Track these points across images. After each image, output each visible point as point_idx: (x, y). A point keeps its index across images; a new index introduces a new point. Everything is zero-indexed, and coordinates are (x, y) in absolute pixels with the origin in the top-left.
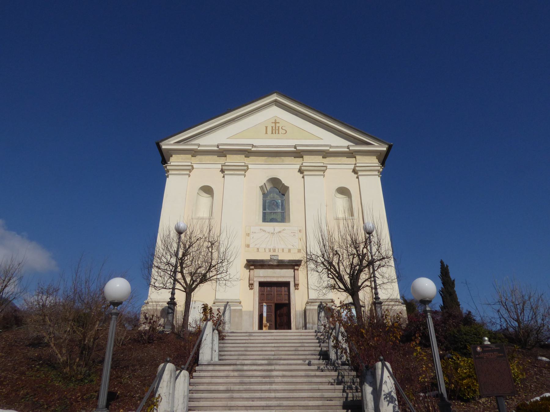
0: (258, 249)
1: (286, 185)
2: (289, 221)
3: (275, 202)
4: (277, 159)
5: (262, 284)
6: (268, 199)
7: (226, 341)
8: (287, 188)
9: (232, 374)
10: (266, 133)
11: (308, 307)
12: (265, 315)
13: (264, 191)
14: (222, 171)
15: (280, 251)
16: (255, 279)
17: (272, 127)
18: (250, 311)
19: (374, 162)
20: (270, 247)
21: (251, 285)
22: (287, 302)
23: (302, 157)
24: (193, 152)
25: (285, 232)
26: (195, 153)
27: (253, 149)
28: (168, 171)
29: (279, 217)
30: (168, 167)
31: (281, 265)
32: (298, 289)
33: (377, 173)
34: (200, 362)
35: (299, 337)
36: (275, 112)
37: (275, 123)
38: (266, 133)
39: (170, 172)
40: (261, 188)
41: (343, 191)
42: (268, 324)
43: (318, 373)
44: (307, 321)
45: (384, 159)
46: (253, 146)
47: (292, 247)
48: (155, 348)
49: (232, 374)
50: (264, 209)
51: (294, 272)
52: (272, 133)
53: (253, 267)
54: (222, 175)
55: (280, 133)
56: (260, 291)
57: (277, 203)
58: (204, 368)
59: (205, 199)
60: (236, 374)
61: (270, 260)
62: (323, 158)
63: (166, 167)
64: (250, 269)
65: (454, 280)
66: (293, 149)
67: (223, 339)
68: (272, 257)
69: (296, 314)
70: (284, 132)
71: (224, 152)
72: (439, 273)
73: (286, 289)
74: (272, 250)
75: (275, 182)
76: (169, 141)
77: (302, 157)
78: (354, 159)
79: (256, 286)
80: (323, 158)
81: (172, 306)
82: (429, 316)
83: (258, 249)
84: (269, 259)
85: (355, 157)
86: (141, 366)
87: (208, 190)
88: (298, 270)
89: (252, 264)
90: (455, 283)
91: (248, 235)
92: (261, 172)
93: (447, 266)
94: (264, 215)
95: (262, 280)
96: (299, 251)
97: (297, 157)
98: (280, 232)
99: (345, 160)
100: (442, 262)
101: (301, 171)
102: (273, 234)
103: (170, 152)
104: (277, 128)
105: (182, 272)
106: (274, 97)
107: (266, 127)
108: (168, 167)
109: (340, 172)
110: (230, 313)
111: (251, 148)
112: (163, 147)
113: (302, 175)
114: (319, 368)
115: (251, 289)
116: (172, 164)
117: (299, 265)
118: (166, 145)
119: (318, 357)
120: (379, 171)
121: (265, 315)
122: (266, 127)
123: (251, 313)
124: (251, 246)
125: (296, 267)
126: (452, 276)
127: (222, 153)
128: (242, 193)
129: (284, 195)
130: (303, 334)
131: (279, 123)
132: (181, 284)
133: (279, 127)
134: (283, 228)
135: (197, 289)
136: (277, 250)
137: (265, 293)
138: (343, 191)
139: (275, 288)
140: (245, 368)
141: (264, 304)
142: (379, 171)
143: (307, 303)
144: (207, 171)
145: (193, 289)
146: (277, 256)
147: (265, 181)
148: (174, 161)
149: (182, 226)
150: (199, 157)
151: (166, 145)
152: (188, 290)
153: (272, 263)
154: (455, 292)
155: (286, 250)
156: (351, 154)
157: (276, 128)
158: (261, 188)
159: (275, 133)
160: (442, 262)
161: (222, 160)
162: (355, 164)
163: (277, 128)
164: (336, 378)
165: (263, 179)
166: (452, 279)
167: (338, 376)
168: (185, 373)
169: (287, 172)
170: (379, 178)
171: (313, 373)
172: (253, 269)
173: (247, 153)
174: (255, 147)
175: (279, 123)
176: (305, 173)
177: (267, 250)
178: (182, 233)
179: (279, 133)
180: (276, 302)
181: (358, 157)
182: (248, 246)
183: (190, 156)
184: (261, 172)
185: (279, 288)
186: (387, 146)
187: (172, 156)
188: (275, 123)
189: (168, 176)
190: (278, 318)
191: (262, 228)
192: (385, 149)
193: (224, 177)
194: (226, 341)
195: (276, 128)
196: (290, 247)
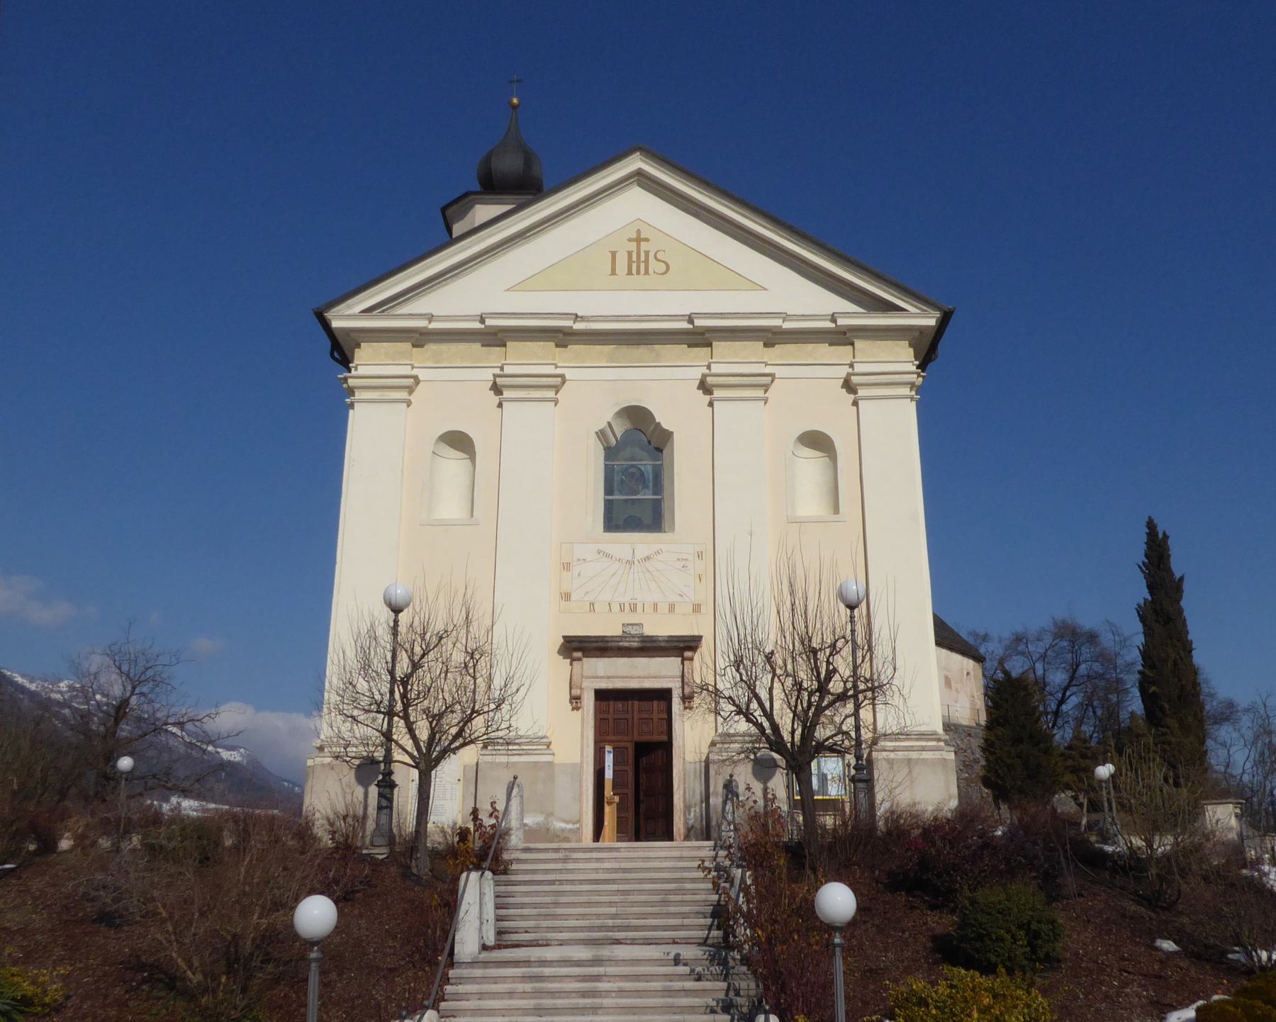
0: (592, 604)
1: (665, 426)
2: (672, 529)
3: (636, 478)
4: (641, 351)
5: (601, 695)
6: (618, 464)
7: (513, 878)
8: (668, 436)
9: (520, 987)
10: (613, 272)
11: (713, 757)
12: (609, 774)
14: (496, 389)
15: (649, 609)
16: (585, 684)
17: (630, 254)
18: (574, 765)
19: (902, 359)
20: (622, 600)
21: (575, 700)
22: (665, 738)
23: (710, 345)
24: (417, 336)
25: (659, 557)
26: (419, 338)
27: (579, 326)
28: (351, 392)
29: (647, 518)
30: (351, 382)
31: (650, 647)
32: (691, 708)
33: (906, 391)
34: (456, 958)
35: (677, 862)
36: (637, 207)
37: (639, 240)
38: (613, 272)
39: (359, 395)
40: (601, 435)
41: (817, 441)
42: (617, 799)
43: (690, 985)
44: (711, 790)
45: (928, 350)
47: (679, 599)
48: (361, 916)
49: (520, 987)
50: (609, 490)
51: (683, 663)
52: (630, 273)
53: (579, 654)
54: (496, 399)
55: (651, 271)
56: (598, 711)
57: (642, 474)
58: (465, 972)
59: (453, 463)
60: (528, 987)
61: (621, 638)
62: (766, 345)
63: (345, 379)
64: (573, 660)
65: (1181, 579)
66: (685, 325)
67: (505, 872)
68: (628, 629)
69: (684, 769)
70: (663, 267)
71: (500, 335)
72: (1141, 557)
73: (663, 704)
74: (627, 606)
75: (637, 417)
76: (349, 307)
77: (710, 345)
78: (850, 348)
79: (589, 701)
80: (766, 345)
81: (387, 790)
82: (838, 953)
83: (592, 604)
84: (619, 633)
85: (852, 344)
86: (340, 974)
87: (459, 442)
88: (691, 659)
89: (576, 647)
90: (1186, 586)
91: (567, 566)
92: (598, 390)
93: (1166, 537)
94: (609, 506)
95: (604, 685)
96: (697, 608)
97: (697, 345)
98: (648, 558)
99: (823, 351)
100: (1151, 525)
101: (704, 387)
102: (630, 563)
103: (353, 335)
104: (643, 258)
105: (406, 717)
106: (635, 163)
107: (614, 254)
108: (351, 382)
109: (807, 387)
110: (522, 803)
112: (335, 324)
113: (708, 398)
114: (692, 971)
115: (576, 708)
116: (362, 371)
117: (694, 649)
118: (344, 318)
119: (709, 921)
120: (912, 385)
121: (609, 774)
122: (614, 254)
123: (577, 769)
124: (574, 597)
125: (688, 654)
126: (1178, 566)
128: (552, 447)
129: (660, 450)
130: (685, 854)
131: (647, 240)
132: (407, 752)
133: (647, 253)
134: (655, 547)
135: (443, 763)
136: (639, 607)
137: (610, 717)
138: (817, 441)
139: (636, 703)
140: (547, 971)
141: (608, 748)
142: (912, 385)
143: (713, 744)
144: (454, 388)
145: (437, 761)
146: (640, 625)
147: (609, 415)
148: (369, 363)
149: (399, 593)
150: (432, 348)
151: (344, 318)
152: (422, 766)
153: (626, 644)
154: (1180, 611)
155: (663, 608)
156: (842, 336)
157: (638, 258)
158: (601, 435)
159: (638, 273)
160: (1151, 525)
161: (494, 355)
162: (851, 366)
163: (643, 258)
164: (722, 996)
165: (604, 413)
166: (1178, 576)
167: (728, 990)
169: (666, 388)
170: (911, 408)
171: (678, 985)
172: (579, 659)
173: (562, 337)
174: (583, 319)
175: (647, 240)
176: (717, 393)
177: (616, 608)
178: (401, 611)
179: (647, 272)
180: (637, 738)
181: (858, 343)
182: (567, 597)
183: (408, 345)
184: (598, 390)
185: (645, 705)
186: (938, 314)
187: (358, 346)
188: (639, 240)
189: (352, 406)
190: (643, 778)
191: (601, 547)
192: (932, 322)
193: (500, 405)
194: (513, 878)
195: (638, 258)
196: (673, 598)
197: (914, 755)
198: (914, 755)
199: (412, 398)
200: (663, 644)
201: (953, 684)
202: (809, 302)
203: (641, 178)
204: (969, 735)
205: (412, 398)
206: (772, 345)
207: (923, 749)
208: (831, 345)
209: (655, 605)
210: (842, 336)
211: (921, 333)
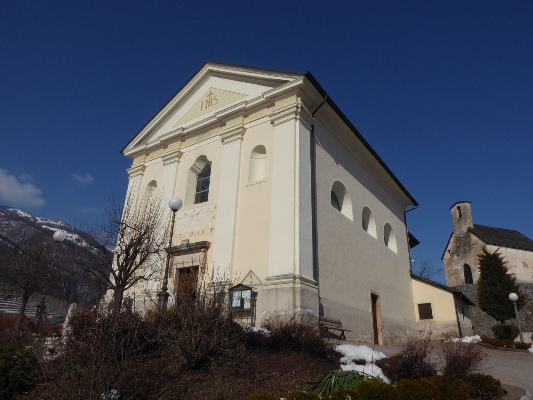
4: (206, 135)
10: (202, 110)
13: (197, 172)
17: (207, 101)
20: (188, 231)
25: (202, 212)
27: (185, 132)
38: (202, 110)
46: (183, 129)
50: (197, 191)
84: (181, 244)
90: (335, 163)
95: (181, 266)
106: (208, 67)
107: (202, 103)
111: (181, 131)
122: (202, 103)
127: (164, 144)
133: (212, 98)
147: (193, 162)
150: (188, 141)
155: (201, 232)
158: (192, 169)
168: (503, 261)
169: (210, 146)
174: (186, 129)
197: (279, 286)
198: (279, 286)
199: (144, 173)
200: (194, 247)
201: (529, 265)
202: (254, 92)
203: (211, 73)
204: (527, 288)
205: (144, 173)
206: (247, 116)
207: (283, 283)
208: (268, 108)
209: (203, 231)
210: (269, 102)
211: (300, 89)
